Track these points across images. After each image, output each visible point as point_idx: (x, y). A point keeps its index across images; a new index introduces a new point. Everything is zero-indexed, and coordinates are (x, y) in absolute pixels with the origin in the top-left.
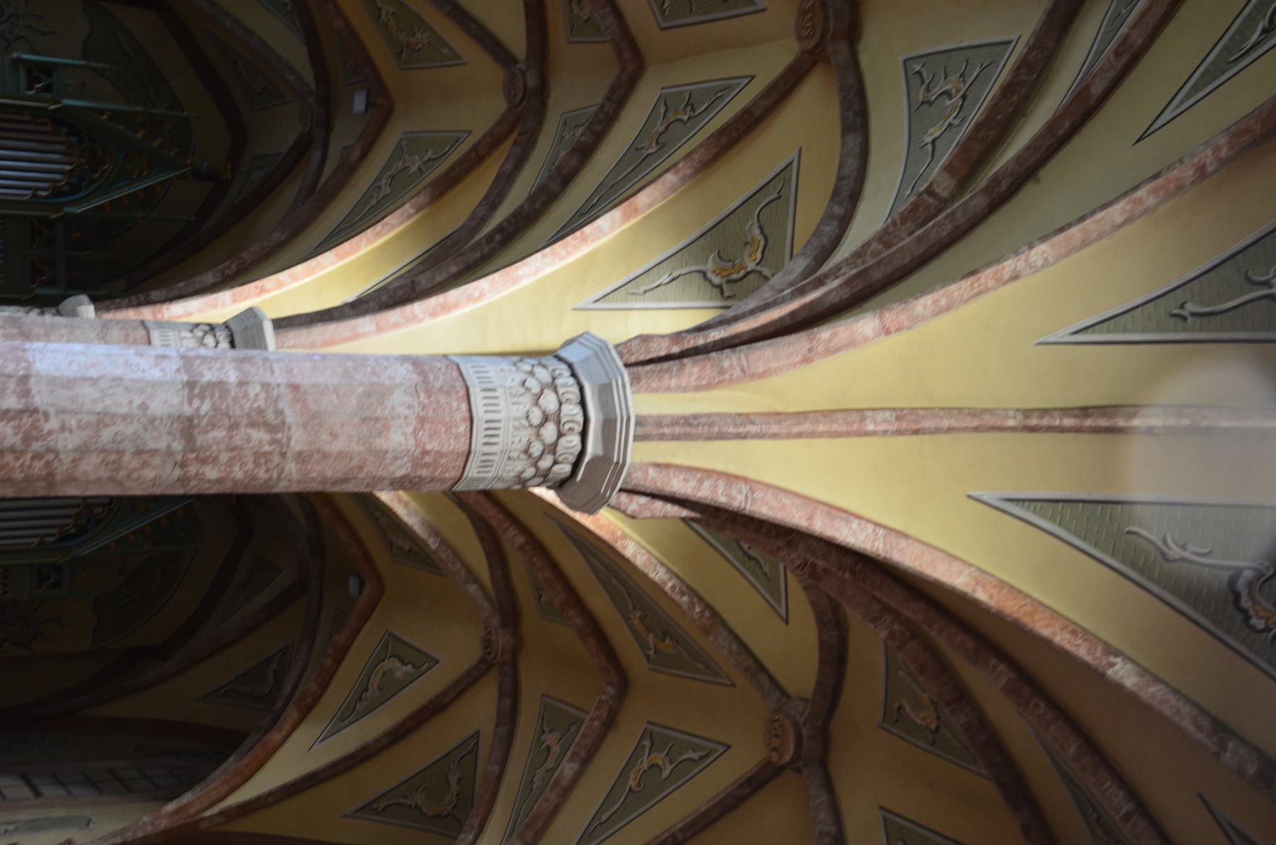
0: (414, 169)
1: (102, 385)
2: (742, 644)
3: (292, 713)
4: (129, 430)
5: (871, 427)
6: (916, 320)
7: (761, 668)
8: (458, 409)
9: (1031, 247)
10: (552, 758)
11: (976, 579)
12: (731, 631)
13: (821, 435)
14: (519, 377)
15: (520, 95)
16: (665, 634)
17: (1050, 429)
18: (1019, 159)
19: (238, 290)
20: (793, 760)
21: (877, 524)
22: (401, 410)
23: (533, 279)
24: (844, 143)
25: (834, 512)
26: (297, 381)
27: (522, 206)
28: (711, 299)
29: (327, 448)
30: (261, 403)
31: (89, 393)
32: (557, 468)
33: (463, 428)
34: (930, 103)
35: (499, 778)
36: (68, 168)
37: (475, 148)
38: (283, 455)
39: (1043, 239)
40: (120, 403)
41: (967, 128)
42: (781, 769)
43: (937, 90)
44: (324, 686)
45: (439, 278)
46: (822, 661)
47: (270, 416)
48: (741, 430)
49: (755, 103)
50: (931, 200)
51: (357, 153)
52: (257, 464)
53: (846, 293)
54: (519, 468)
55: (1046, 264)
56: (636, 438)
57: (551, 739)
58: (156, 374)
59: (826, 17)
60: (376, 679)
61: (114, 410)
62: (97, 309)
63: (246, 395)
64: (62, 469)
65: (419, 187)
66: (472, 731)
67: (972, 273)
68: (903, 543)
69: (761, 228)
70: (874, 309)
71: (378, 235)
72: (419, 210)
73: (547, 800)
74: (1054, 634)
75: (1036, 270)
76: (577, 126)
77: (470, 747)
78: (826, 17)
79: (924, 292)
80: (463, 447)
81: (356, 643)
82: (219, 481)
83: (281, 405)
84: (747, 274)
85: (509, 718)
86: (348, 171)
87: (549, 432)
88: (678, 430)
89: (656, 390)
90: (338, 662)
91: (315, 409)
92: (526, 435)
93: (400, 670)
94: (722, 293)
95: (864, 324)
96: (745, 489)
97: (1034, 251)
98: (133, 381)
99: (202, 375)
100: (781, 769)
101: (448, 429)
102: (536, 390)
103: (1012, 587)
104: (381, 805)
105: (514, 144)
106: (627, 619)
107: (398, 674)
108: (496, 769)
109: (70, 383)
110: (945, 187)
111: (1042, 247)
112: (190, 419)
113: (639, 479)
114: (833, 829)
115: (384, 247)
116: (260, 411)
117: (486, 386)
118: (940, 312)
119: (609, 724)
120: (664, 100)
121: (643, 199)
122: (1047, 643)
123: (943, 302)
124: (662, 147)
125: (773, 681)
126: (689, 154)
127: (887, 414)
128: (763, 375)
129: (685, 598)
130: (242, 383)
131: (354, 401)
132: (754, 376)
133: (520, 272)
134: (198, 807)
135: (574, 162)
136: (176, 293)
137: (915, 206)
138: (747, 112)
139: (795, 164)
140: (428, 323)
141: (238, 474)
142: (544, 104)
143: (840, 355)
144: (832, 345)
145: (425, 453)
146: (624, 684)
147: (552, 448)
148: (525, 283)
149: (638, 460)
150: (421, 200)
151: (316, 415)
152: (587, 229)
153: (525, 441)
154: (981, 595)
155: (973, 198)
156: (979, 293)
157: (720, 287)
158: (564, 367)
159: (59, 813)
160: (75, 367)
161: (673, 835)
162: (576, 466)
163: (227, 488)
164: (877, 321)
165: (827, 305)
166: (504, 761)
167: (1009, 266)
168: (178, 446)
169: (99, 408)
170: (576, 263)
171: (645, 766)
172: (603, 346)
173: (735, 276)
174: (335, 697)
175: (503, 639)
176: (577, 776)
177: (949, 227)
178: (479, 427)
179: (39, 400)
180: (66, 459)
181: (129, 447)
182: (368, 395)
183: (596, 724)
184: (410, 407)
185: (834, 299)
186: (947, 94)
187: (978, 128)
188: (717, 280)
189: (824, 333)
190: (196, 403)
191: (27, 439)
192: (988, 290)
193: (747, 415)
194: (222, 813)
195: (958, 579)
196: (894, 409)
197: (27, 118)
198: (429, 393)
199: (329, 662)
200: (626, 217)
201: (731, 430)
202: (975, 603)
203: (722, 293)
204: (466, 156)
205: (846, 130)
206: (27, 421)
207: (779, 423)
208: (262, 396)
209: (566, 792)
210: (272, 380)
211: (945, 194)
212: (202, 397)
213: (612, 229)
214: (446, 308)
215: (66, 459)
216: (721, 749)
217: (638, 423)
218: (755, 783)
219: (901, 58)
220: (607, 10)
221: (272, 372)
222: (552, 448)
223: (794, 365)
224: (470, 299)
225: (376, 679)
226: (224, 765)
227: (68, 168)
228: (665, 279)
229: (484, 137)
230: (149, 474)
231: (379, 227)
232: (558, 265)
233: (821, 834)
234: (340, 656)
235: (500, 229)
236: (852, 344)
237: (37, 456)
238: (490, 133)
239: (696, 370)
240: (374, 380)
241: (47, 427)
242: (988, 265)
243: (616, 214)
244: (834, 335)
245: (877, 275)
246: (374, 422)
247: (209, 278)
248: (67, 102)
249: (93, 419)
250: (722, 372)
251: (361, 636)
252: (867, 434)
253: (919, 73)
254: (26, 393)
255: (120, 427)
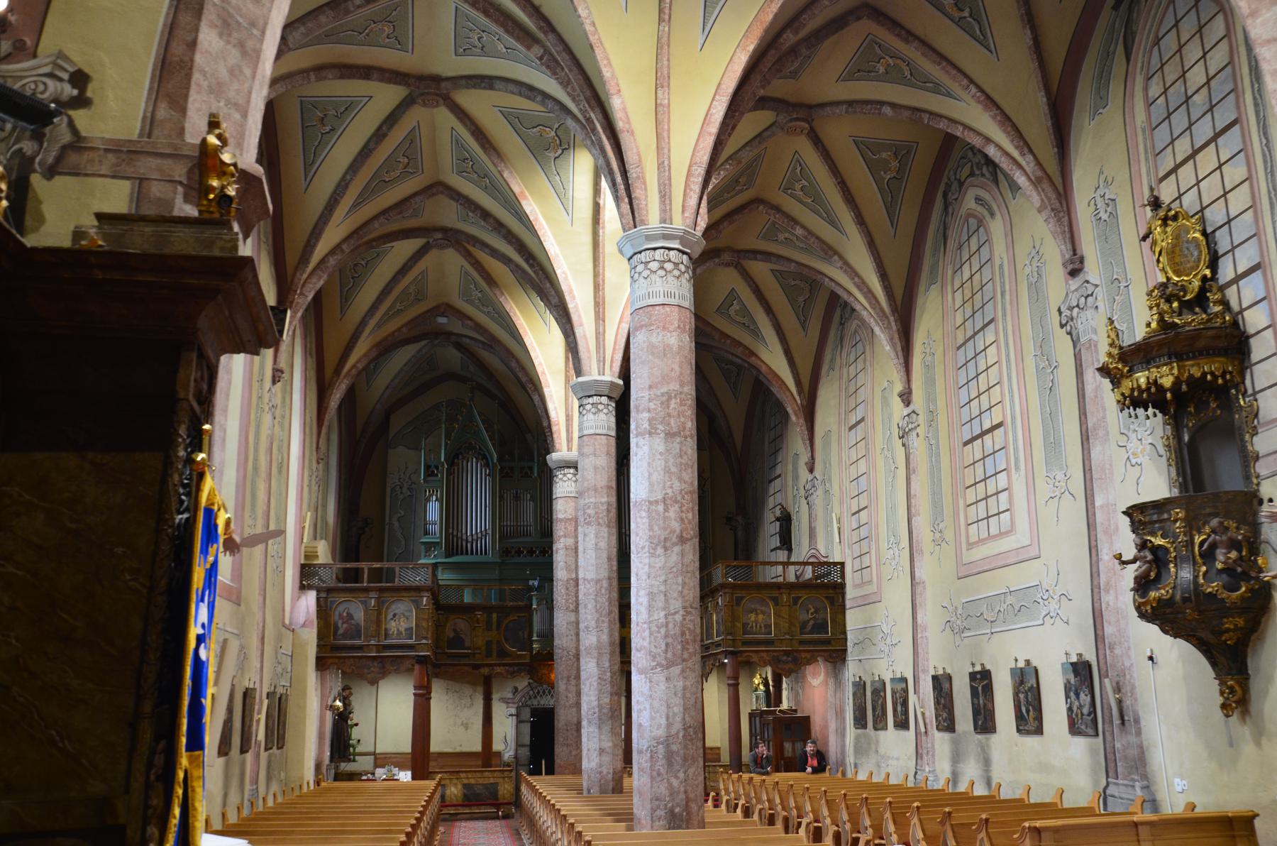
0: (480, 295)
1: (652, 471)
2: (746, 144)
3: (753, 360)
4: (672, 460)
5: (666, 101)
6: (613, 76)
7: (759, 135)
8: (658, 311)
9: (579, 16)
10: (791, 238)
11: (743, 50)
12: (739, 150)
13: (669, 127)
14: (641, 280)
15: (446, 242)
16: (737, 181)
17: (670, 9)
18: (530, 16)
19: (543, 385)
20: (808, 123)
21: (713, 99)
22: (660, 338)
23: (556, 246)
24: (500, 90)
25: (707, 122)
26: (647, 386)
27: (515, 248)
28: (569, 155)
29: (678, 373)
30: (658, 402)
31: (655, 477)
32: (685, 263)
33: (668, 309)
34: (483, 47)
35: (797, 262)
36: (474, 460)
37: (472, 265)
38: (681, 393)
39: (576, 10)
40: (660, 463)
41: (501, 31)
42: (811, 127)
43: (477, 43)
44: (740, 344)
45: (553, 293)
46: (762, 109)
47: (664, 399)
48: (667, 169)
49: (469, 130)
50: (545, 58)
51: (469, 322)
52: (685, 405)
53: (598, 110)
54: (685, 281)
55: (587, 8)
56: (671, 224)
57: (781, 237)
58: (646, 448)
59: (428, 94)
60: (739, 319)
61: (663, 467)
62: (553, 452)
63: (655, 409)
64: (688, 488)
65: (492, 295)
66: (770, 272)
67: (592, 48)
68: (723, 86)
69: (533, 128)
70: (608, 99)
71: (515, 314)
72: (503, 294)
73: (814, 243)
74: (772, 12)
75: (590, 13)
76: (468, 215)
77: (780, 276)
78: (428, 94)
79: (600, 72)
80: (677, 308)
81: (718, 327)
82: (692, 421)
83: (659, 394)
84: (557, 135)
85: (767, 256)
86: (479, 327)
87: (669, 266)
88: (667, 202)
89: (647, 211)
90: (729, 337)
91: (660, 378)
92: (670, 278)
93: (736, 306)
94: (566, 149)
95: (616, 104)
96: (694, 168)
97: (582, 15)
98: (649, 458)
99: (645, 428)
100: (812, 129)
101: (668, 316)
102: (648, 272)
103: (747, 31)
104: (802, 318)
105: (474, 247)
106: (728, 200)
107: (738, 308)
108: (793, 264)
109: (651, 484)
110: (537, 50)
111: (580, 11)
112: (666, 434)
113: (690, 221)
114: (844, 107)
115: (521, 311)
116: (662, 403)
117: (647, 297)
118: (610, 64)
119: (777, 209)
120: (460, 173)
121: (516, 189)
122: (776, 15)
123: (605, 62)
124: (486, 176)
125: (766, 130)
126: (494, 165)
127: (660, 93)
128: (639, 155)
129: (722, 173)
130: (649, 411)
131: (656, 360)
132: (640, 161)
133: (553, 253)
134: (795, 406)
135: (491, 220)
136: (544, 414)
137: (548, 67)
138: (473, 134)
139: (501, 109)
140: (578, 300)
141: (689, 413)
142: (451, 229)
143: (630, 116)
144: (626, 120)
145: (679, 327)
146: (758, 201)
147: (676, 265)
148: (558, 251)
149: (681, 222)
150: (498, 292)
151: (663, 379)
152: (531, 218)
153: (673, 278)
154: (751, 48)
155: (549, 41)
156: (601, 42)
157: (563, 150)
158: (636, 256)
159: (790, 467)
160: (643, 482)
161: (839, 183)
162: (684, 253)
163: (694, 417)
164: (614, 97)
165: (603, 120)
166: (789, 260)
167: (588, 28)
168: (678, 440)
169: (662, 473)
170: (547, 224)
171: (801, 193)
172: (626, 237)
173: (558, 142)
174: (746, 339)
175: (726, 257)
176: (803, 227)
177: (564, 54)
178: (666, 301)
179: (660, 497)
180: (684, 486)
181: (679, 460)
182: (653, 354)
183: (777, 216)
184: (658, 334)
185: (600, 116)
186: (479, 39)
187: (507, 31)
188: (560, 152)
189: (620, 125)
190: (659, 431)
191: (676, 502)
192: (599, 39)
193: (659, 165)
194: (800, 394)
195: (742, 60)
196: (656, 88)
197: (452, 477)
198: (651, 325)
199: (729, 341)
200: (526, 198)
201: (667, 174)
202: (755, 50)
203: (566, 149)
204: (476, 269)
205: (491, 88)
206: (668, 502)
207: (663, 148)
208: (655, 402)
209: (810, 233)
210: (647, 397)
211: (542, 51)
212: (656, 429)
213: (531, 205)
214: (571, 292)
215: (684, 486)
216: (797, 155)
217: (664, 222)
218: (817, 141)
219: (454, 57)
220: (412, 200)
221: (643, 397)
222: (676, 265)
223: (635, 140)
224: (566, 278)
225: (739, 319)
226: (775, 392)
227: (474, 460)
228: (558, 178)
229: (467, 260)
230: (690, 452)
231: (511, 314)
232: (549, 233)
233: (847, 112)
234: (725, 335)
235: (527, 261)
236: (624, 109)
237: (683, 498)
238: (464, 257)
239: (638, 191)
240: (645, 350)
241: (671, 494)
242: (588, 39)
243: (524, 203)
244: (621, 119)
245: (588, 93)
246: (666, 350)
247: (536, 398)
248: (443, 459)
249: (667, 475)
250: (638, 177)
251: (715, 325)
252: (669, 104)
253: (464, 50)
254: (656, 502)
255: (670, 463)
